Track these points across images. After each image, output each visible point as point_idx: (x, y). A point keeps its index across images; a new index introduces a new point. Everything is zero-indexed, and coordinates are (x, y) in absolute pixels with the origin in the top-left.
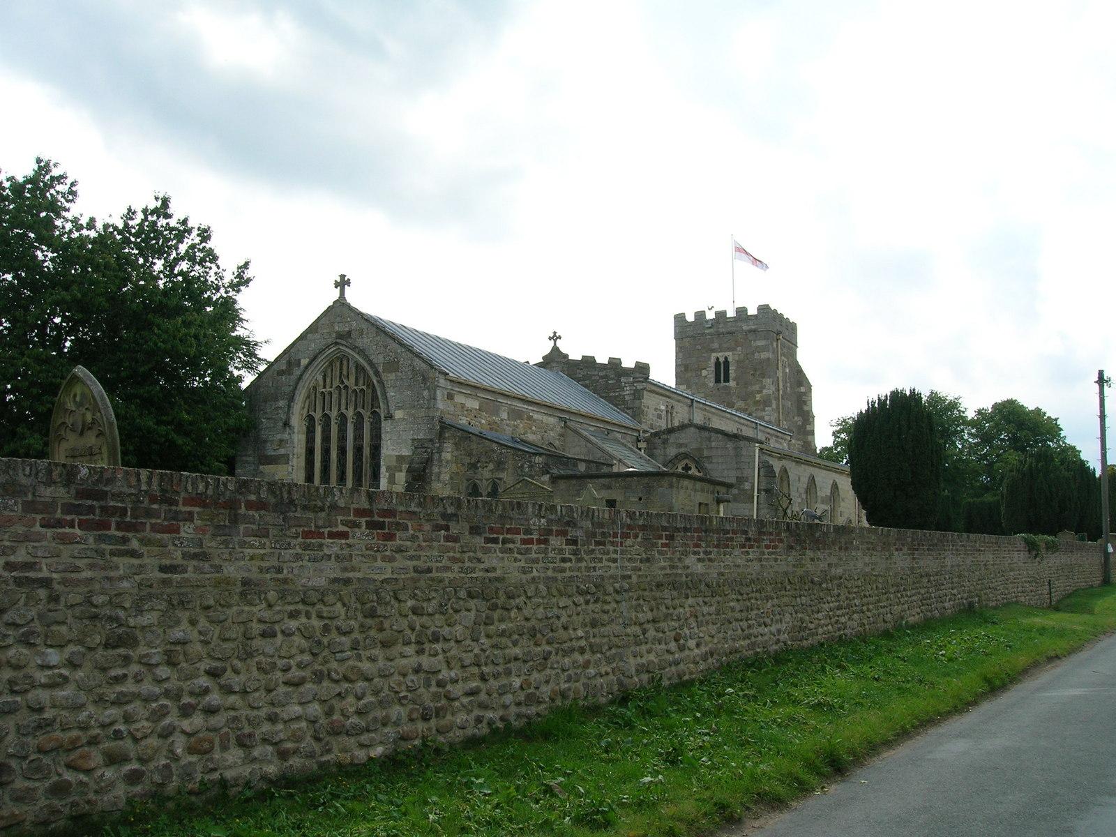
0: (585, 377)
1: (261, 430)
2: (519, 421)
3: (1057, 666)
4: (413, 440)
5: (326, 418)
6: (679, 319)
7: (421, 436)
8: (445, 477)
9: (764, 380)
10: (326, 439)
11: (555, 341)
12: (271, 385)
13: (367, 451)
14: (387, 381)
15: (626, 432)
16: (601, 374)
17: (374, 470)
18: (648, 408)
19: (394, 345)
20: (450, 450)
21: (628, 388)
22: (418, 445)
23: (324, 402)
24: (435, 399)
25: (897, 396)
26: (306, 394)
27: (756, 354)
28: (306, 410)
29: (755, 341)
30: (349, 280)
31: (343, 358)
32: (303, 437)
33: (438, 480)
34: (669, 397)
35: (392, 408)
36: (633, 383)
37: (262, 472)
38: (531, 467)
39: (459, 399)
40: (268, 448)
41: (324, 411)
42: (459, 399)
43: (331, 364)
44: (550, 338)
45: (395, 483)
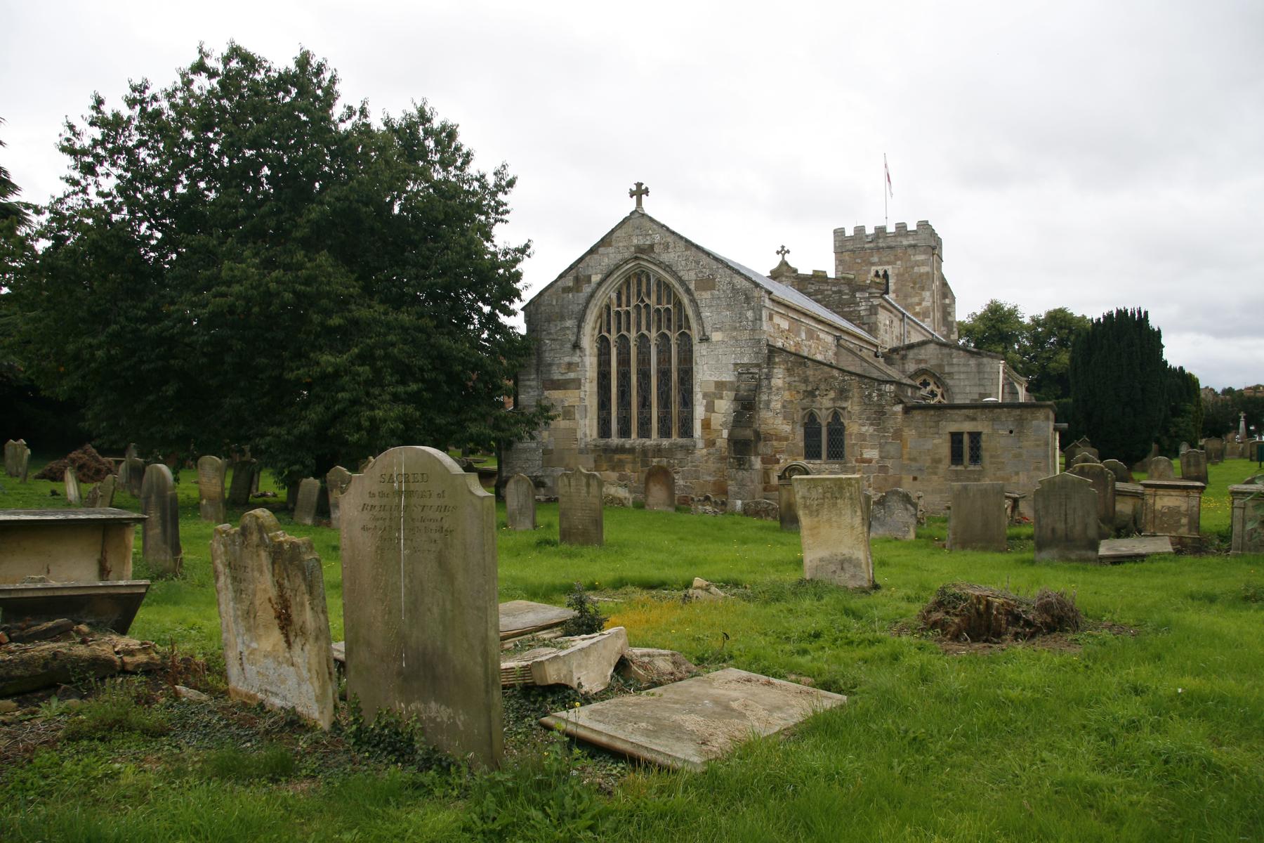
0: (817, 292)
1: (545, 351)
3: (1083, 569)
4: (736, 364)
5: (623, 340)
6: (839, 233)
7: (746, 360)
8: (776, 405)
9: (923, 293)
11: (783, 255)
12: (554, 303)
14: (701, 300)
16: (834, 289)
19: (705, 260)
20: (781, 376)
21: (864, 304)
22: (743, 371)
24: (761, 320)
25: (1122, 314)
27: (916, 268)
28: (597, 332)
29: (914, 255)
30: (647, 189)
32: (594, 360)
34: (891, 312)
36: (869, 298)
38: (880, 396)
43: (628, 282)
44: (778, 253)
45: (714, 412)
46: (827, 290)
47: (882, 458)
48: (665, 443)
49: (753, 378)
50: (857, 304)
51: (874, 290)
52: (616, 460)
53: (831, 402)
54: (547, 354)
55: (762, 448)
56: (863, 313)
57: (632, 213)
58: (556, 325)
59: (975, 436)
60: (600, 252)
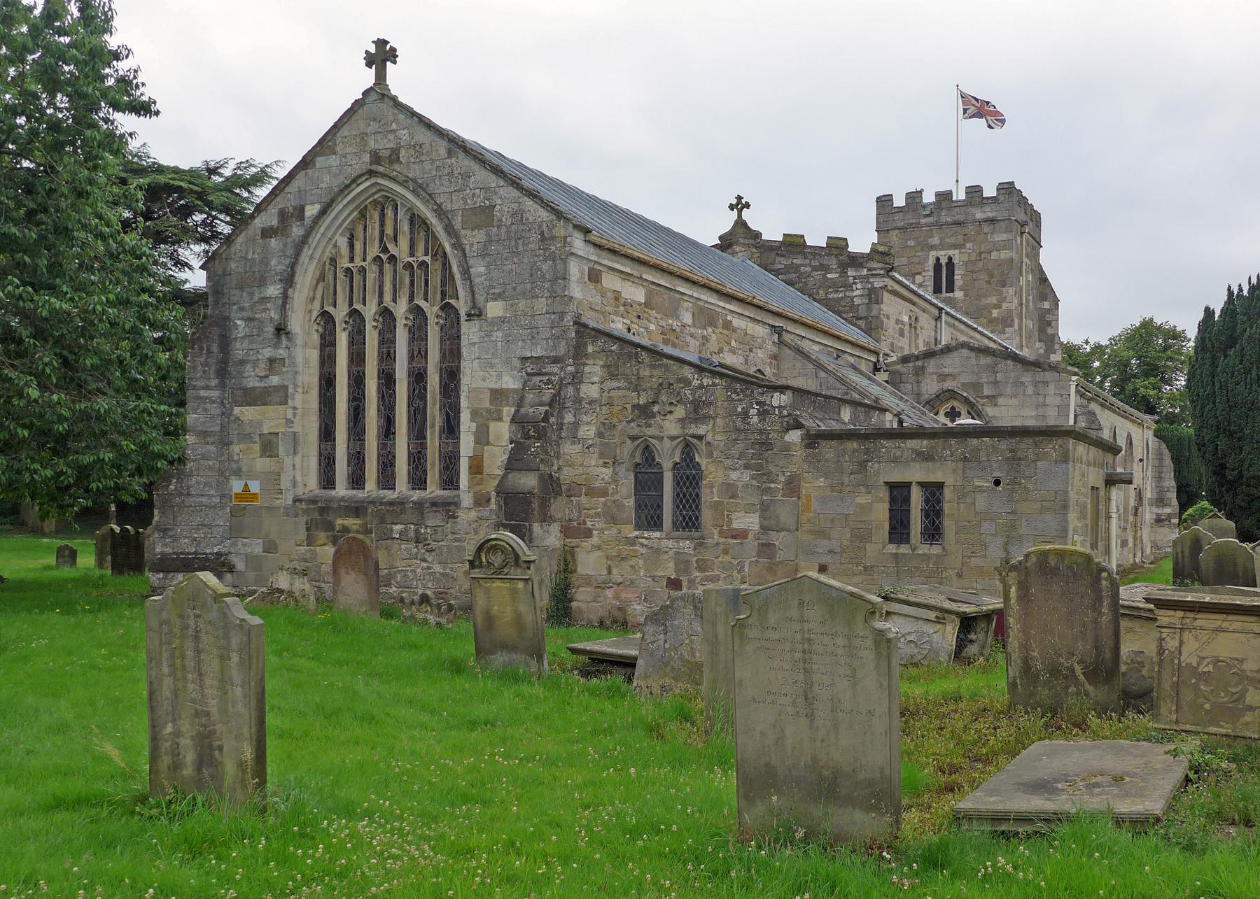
2: (710, 330)
6: (884, 202)
7: (538, 352)
10: (357, 358)
13: (433, 381)
14: (472, 245)
15: (861, 355)
17: (448, 415)
18: (888, 318)
20: (596, 379)
21: (859, 286)
23: (351, 287)
26: (318, 273)
31: (385, 203)
32: (314, 355)
33: (575, 439)
34: (914, 303)
35: (480, 299)
37: (238, 418)
38: (763, 414)
39: (609, 281)
40: (246, 374)
41: (351, 304)
42: (609, 281)
43: (363, 215)
45: (488, 443)
46: (805, 266)
47: (765, 529)
48: (416, 495)
49: (549, 382)
50: (849, 287)
51: (875, 265)
52: (337, 528)
53: (679, 426)
54: (238, 345)
55: (558, 507)
56: (857, 301)
57: (366, 93)
58: (252, 294)
59: (933, 491)
60: (318, 165)
